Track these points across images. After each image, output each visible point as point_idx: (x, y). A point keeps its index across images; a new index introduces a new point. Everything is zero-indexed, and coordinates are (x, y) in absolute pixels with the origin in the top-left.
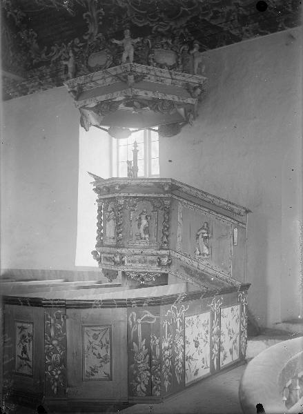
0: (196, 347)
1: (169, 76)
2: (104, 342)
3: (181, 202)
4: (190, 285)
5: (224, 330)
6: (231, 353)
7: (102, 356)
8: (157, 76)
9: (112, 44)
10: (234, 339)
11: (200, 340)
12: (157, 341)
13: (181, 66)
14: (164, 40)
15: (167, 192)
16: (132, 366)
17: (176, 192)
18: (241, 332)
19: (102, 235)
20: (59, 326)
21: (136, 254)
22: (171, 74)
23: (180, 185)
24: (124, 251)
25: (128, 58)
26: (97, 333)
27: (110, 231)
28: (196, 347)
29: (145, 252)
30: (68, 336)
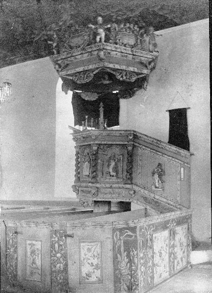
0: (160, 257)
1: (130, 53)
2: (95, 254)
3: (140, 148)
4: (148, 210)
5: (177, 243)
6: (182, 260)
7: (94, 265)
8: (122, 52)
9: (88, 27)
10: (183, 250)
11: (162, 252)
12: (135, 253)
13: (140, 46)
14: (128, 25)
15: (131, 140)
16: (117, 272)
17: (138, 141)
18: (188, 245)
19: (79, 173)
20: (61, 243)
21: (107, 188)
22: (132, 51)
23: (140, 135)
24: (98, 185)
25: (100, 39)
26: (90, 247)
27: (86, 171)
28: (160, 257)
29: (114, 186)
30: (19, 259)
